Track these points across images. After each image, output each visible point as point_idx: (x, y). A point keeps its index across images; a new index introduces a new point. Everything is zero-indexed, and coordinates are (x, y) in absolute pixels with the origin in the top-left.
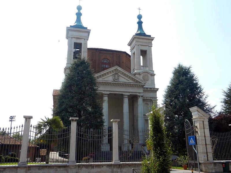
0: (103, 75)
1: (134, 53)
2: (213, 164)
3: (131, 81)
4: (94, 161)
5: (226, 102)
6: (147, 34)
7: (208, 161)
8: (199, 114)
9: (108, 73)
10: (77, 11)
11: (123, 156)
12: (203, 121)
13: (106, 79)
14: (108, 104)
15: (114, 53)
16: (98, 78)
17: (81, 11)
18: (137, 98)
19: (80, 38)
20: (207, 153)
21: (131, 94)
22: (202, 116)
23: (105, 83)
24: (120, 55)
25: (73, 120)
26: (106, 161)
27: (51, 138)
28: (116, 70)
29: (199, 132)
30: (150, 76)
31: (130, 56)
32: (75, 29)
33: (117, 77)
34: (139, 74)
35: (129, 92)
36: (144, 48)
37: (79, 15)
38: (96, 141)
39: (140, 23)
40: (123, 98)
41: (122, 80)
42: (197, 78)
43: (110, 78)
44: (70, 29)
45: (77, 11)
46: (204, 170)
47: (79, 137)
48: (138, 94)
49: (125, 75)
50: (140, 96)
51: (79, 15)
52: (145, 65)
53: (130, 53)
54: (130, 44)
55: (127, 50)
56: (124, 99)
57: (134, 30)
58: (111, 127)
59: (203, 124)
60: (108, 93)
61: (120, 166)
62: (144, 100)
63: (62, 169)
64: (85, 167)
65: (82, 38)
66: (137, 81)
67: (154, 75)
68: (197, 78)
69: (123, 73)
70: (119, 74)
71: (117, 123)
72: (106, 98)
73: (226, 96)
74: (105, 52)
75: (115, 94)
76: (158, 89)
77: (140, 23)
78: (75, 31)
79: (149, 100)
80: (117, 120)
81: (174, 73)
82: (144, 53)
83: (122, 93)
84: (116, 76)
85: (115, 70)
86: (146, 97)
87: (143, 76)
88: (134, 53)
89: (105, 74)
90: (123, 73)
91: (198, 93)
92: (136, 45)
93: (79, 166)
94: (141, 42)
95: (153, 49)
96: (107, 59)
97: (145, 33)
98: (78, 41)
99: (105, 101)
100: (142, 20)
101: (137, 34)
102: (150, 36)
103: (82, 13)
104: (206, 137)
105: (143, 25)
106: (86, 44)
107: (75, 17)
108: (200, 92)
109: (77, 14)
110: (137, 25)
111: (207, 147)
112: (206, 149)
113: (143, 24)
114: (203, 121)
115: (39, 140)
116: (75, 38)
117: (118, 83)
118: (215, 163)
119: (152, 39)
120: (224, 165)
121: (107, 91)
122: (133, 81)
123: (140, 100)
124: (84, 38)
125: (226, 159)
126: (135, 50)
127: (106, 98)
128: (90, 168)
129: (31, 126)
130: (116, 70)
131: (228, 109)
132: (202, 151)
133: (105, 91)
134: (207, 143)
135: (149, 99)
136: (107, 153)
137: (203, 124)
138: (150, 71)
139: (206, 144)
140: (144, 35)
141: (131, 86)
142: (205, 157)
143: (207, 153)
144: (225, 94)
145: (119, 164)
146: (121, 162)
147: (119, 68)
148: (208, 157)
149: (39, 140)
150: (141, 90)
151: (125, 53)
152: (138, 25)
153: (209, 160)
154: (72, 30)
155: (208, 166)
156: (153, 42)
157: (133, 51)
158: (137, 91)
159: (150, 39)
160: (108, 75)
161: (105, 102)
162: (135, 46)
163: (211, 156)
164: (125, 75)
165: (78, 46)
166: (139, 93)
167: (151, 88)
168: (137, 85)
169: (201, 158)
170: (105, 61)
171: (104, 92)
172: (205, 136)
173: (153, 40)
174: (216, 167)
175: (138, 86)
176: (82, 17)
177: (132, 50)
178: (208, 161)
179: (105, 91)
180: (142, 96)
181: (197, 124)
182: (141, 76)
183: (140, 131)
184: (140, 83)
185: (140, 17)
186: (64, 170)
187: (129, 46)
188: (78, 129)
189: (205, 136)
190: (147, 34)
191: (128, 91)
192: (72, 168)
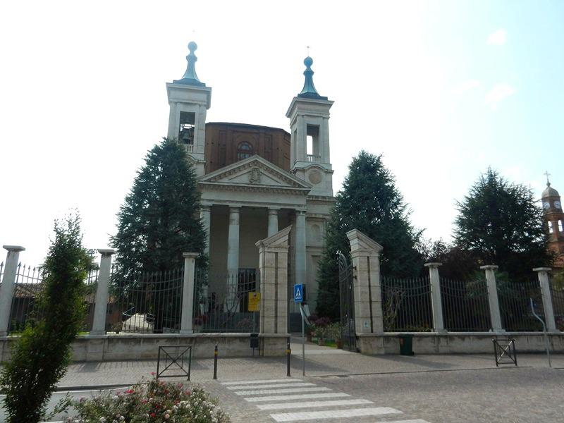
0: (230, 173)
1: (296, 132)
2: (382, 339)
3: (283, 184)
4: (157, 330)
5: (462, 223)
6: (321, 95)
7: (372, 332)
8: (361, 243)
9: (239, 168)
10: (188, 52)
11: (198, 320)
12: (368, 257)
13: (236, 181)
14: (238, 226)
16: (221, 179)
17: (196, 53)
18: (295, 215)
19: (192, 104)
20: (371, 317)
21: (282, 207)
22: (367, 247)
24: (272, 136)
26: (398, 329)
27: (158, 289)
28: (256, 162)
29: (358, 278)
30: (323, 174)
31: (289, 135)
32: (182, 86)
33: (257, 176)
34: (303, 170)
35: (280, 204)
36: (314, 122)
37: (192, 60)
39: (309, 74)
40: (268, 215)
41: (267, 181)
42: (395, 176)
43: (243, 179)
44: (173, 88)
46: (362, 349)
48: (297, 208)
49: (272, 171)
50: (299, 212)
51: (192, 60)
52: (315, 155)
53: (289, 131)
54: (289, 115)
55: (285, 124)
56: (270, 217)
57: (298, 87)
58: (254, 270)
59: (368, 262)
60: (240, 205)
62: (309, 219)
64: (122, 342)
65: (196, 104)
66: (295, 183)
67: (332, 172)
68: (395, 176)
69: (267, 169)
70: (262, 170)
71: (191, 259)
72: (235, 216)
73: (463, 212)
75: (254, 208)
77: (309, 74)
78: (181, 90)
79: (319, 220)
80: (194, 254)
81: (350, 167)
82: (314, 131)
83: (266, 206)
84: (256, 174)
85: (253, 162)
86: (316, 214)
87: (310, 177)
88: (296, 132)
89: (234, 170)
90: (267, 169)
91: (396, 204)
92: (298, 115)
93: (110, 340)
94: (307, 110)
95: (332, 124)
96: (246, 142)
97: (316, 94)
98: (188, 109)
99: (233, 220)
100: (312, 67)
101: (300, 96)
102: (326, 98)
103: (197, 56)
104: (372, 288)
105: (315, 78)
106: (203, 116)
108: (398, 203)
110: (304, 77)
111: (373, 307)
112: (371, 311)
113: (314, 77)
114: (368, 257)
115: (177, 291)
117: (258, 188)
118: (387, 338)
119: (330, 104)
121: (237, 202)
122: (288, 183)
123: (301, 220)
124: (199, 103)
125: (471, 329)
126: (296, 126)
127: (235, 216)
128: (132, 343)
129: (20, 265)
130: (256, 162)
131: (463, 235)
132: (361, 314)
133: (233, 202)
134: (373, 299)
135: (321, 216)
137: (368, 262)
138: (323, 165)
139: (371, 302)
140: (316, 96)
141: (283, 193)
142: (367, 325)
143: (371, 317)
144: (460, 208)
145: (189, 336)
147: (261, 160)
148: (374, 325)
149: (177, 291)
150: (302, 201)
151: (282, 131)
153: (374, 331)
154: (175, 89)
155: (371, 343)
156: (331, 110)
158: (295, 202)
159: (326, 104)
160: (241, 173)
161: (233, 222)
163: (378, 323)
164: (272, 171)
165: (187, 117)
166: (299, 206)
167: (324, 197)
168: (295, 191)
169: (361, 327)
170: (244, 148)
171: (230, 205)
172: (370, 286)
173: (330, 105)
174: (389, 345)
175: (297, 192)
176: (314, 77)
177: (292, 124)
178: (372, 332)
179: (233, 202)
180: (304, 212)
181: (356, 262)
182: (307, 174)
183: (231, 276)
184: (300, 186)
186: (80, 347)
189: (370, 286)
191: (235, 200)
192: (95, 342)
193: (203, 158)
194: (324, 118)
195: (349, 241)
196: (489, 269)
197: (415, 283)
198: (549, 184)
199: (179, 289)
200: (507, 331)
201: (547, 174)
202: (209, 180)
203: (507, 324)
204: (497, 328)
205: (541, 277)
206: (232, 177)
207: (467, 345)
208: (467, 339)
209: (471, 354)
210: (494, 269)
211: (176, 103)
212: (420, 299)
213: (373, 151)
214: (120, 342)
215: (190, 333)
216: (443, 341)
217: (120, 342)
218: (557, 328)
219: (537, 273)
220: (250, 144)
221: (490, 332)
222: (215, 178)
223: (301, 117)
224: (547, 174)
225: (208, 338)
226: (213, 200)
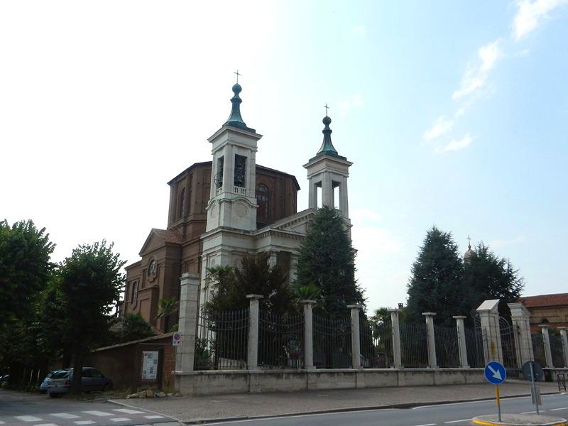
1: (221, 160)
6: (249, 125)
15: (278, 176)
23: (296, 236)
25: (253, 298)
38: (230, 331)
39: (236, 102)
45: (324, 126)
47: (262, 328)
54: (307, 167)
57: (316, 145)
60: (279, 250)
61: (470, 372)
63: (429, 375)
74: (342, 195)
76: (357, 251)
77: (236, 102)
88: (221, 160)
92: (227, 144)
98: (242, 153)
100: (241, 95)
105: (332, 136)
106: (254, 159)
107: (229, 107)
109: (233, 100)
110: (231, 104)
113: (241, 105)
116: (236, 146)
119: (350, 164)
120: (547, 373)
121: (278, 247)
126: (224, 153)
136: (447, 358)
146: (405, 367)
152: (323, 135)
157: (219, 155)
162: (224, 146)
175: (280, 234)
176: (242, 106)
185: (237, 89)
187: (211, 142)
188: (261, 316)
190: (339, 154)
193: (256, 203)
194: (344, 177)
195: (509, 309)
196: (430, 316)
197: (241, 314)
198: (470, 247)
199: (247, 327)
200: (317, 368)
201: (469, 239)
202: (278, 228)
203: (262, 360)
204: (466, 367)
205: (458, 323)
206: (294, 226)
207: (283, 383)
208: (408, 374)
209: (373, 388)
210: (434, 317)
211: (232, 145)
212: (234, 334)
213: (443, 229)
214: (291, 377)
215: (257, 370)
216: (401, 376)
217: (291, 377)
218: (554, 365)
219: (350, 309)
220: (267, 186)
221: (428, 368)
222: (282, 227)
223: (230, 147)
224: (469, 239)
225: (476, 371)
226: (280, 247)
